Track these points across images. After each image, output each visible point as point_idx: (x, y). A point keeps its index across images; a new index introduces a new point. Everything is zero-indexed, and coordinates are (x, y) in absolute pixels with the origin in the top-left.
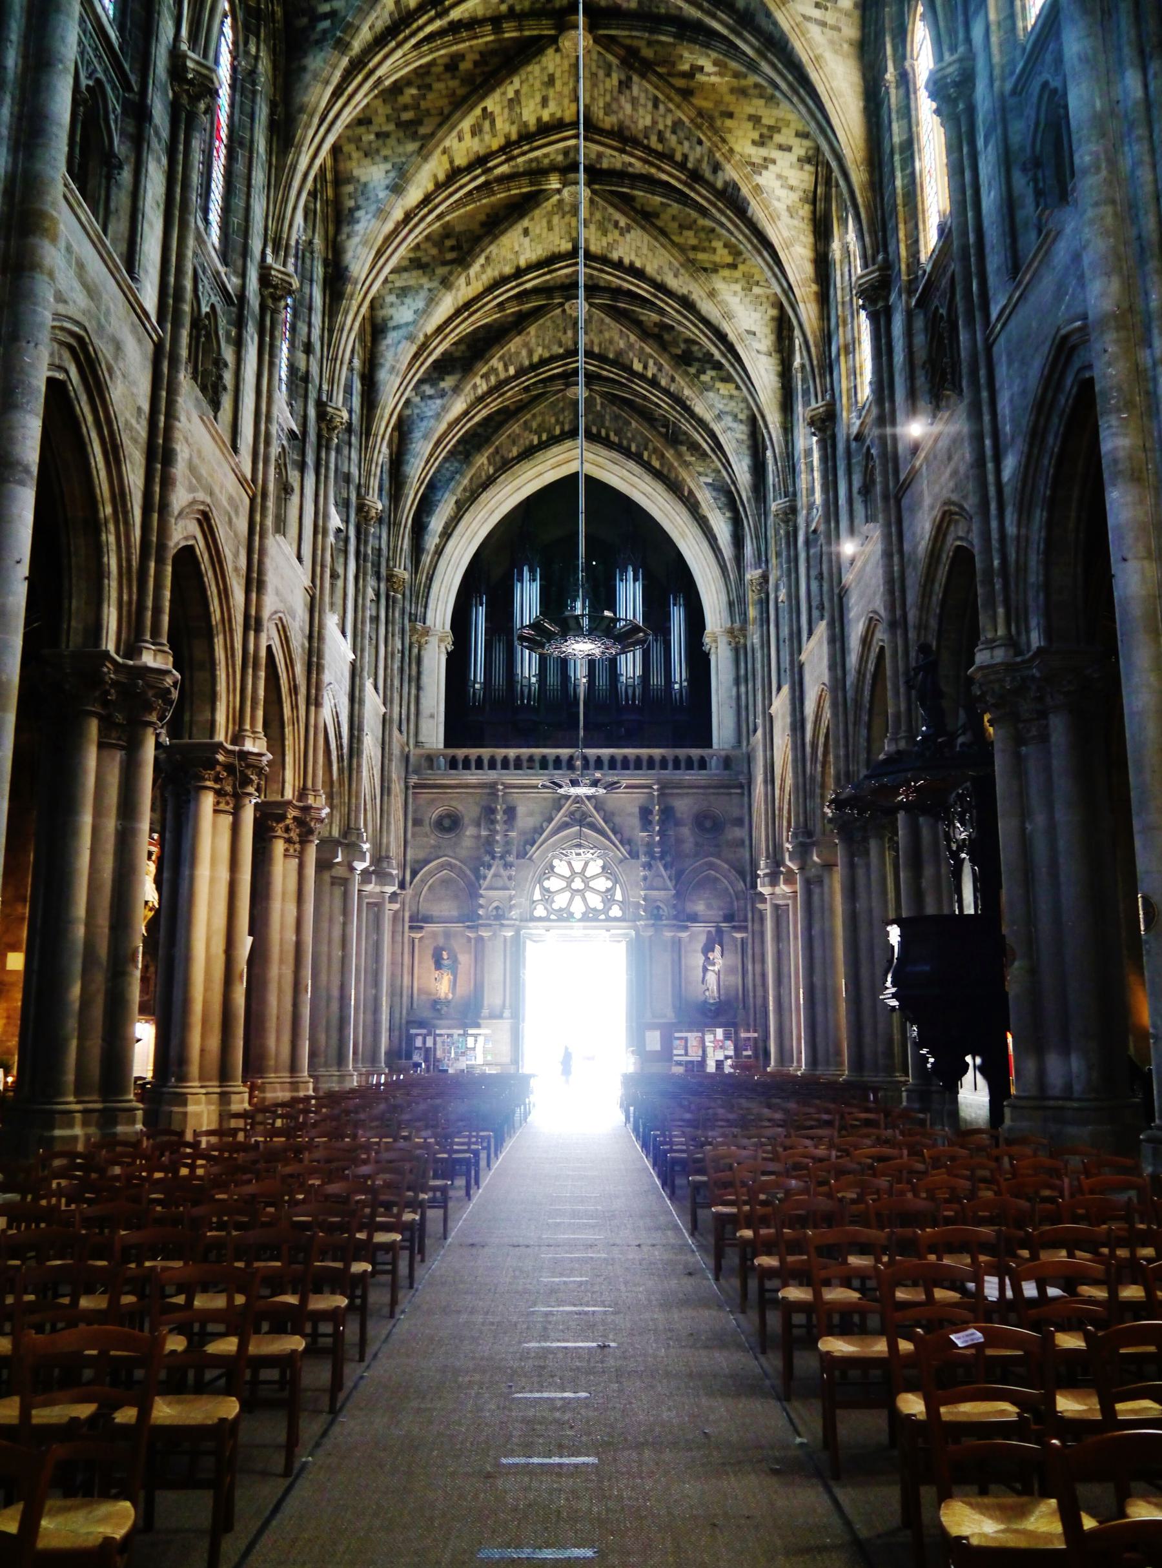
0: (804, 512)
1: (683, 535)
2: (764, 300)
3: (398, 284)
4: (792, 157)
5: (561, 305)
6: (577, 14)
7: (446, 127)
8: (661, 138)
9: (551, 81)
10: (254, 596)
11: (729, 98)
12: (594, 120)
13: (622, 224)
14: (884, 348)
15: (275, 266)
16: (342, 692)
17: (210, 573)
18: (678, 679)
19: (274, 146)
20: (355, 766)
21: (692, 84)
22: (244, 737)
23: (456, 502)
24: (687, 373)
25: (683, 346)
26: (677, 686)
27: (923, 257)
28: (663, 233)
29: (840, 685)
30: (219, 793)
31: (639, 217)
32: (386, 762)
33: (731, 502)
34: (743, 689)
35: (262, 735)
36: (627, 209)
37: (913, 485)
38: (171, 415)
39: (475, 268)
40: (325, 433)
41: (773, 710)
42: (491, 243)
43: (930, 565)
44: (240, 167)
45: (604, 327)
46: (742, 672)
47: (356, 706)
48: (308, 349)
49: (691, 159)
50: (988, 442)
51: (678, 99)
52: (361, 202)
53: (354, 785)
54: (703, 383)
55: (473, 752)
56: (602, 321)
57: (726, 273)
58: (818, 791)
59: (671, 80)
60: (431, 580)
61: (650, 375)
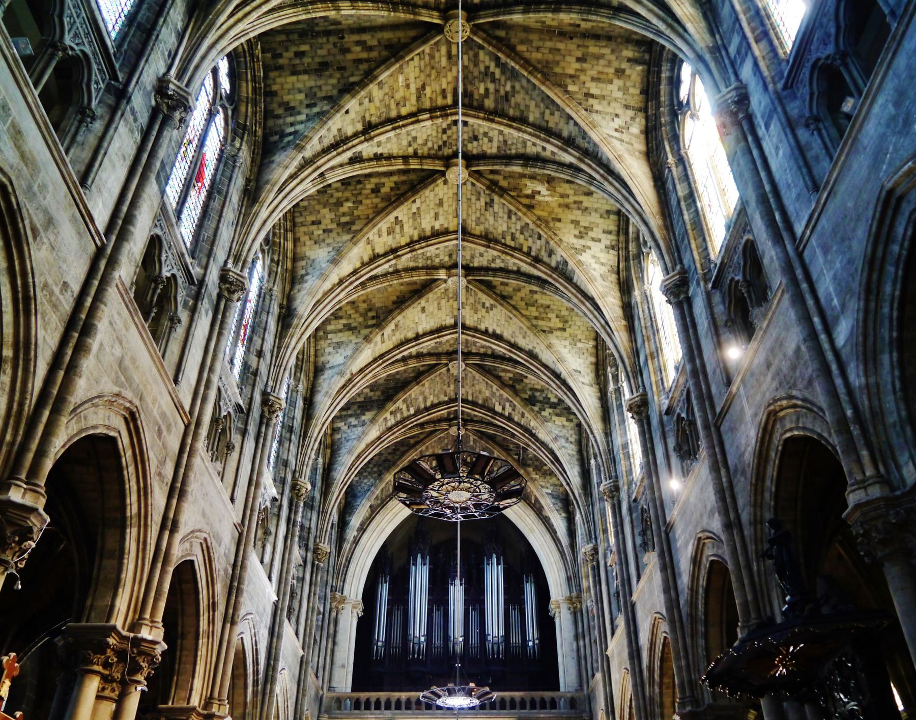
0: (626, 487)
1: (532, 530)
2: (585, 351)
3: (334, 340)
4: (602, 245)
5: (447, 365)
6: (457, 8)
7: (370, 225)
8: (513, 239)
9: (441, 203)
10: (175, 502)
11: (558, 210)
12: (469, 229)
13: (487, 305)
14: (689, 324)
15: (233, 269)
16: (263, 625)
17: (131, 469)
18: (531, 638)
19: (245, 203)
20: (268, 691)
21: (533, 202)
22: (141, 625)
23: (371, 507)
24: (533, 410)
25: (529, 393)
26: (531, 644)
27: (712, 257)
28: (515, 308)
29: (674, 604)
30: (105, 679)
31: (499, 298)
32: (300, 696)
33: (566, 504)
34: (581, 643)
35: (161, 625)
36: (491, 293)
37: (731, 410)
38: (98, 298)
39: (388, 331)
40: (266, 414)
41: (609, 653)
42: (399, 313)
43: (759, 464)
44: (216, 204)
45: (476, 382)
46: (580, 630)
47: (275, 640)
48: (260, 354)
49: (534, 249)
50: (816, 320)
51: (524, 210)
52: (310, 270)
53: (265, 708)
54: (543, 417)
55: (373, 695)
56: (474, 377)
57: (559, 333)
58: (657, 710)
59: (519, 199)
60: (349, 562)
61: (507, 414)
